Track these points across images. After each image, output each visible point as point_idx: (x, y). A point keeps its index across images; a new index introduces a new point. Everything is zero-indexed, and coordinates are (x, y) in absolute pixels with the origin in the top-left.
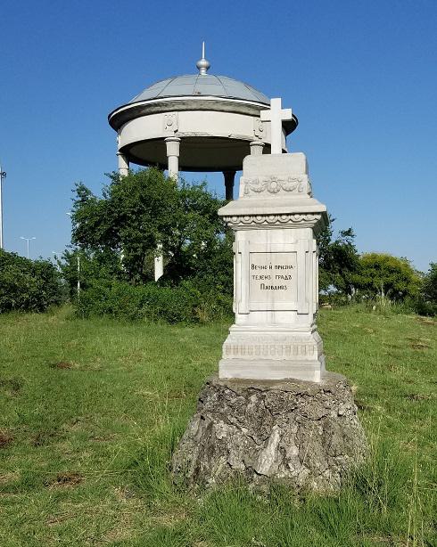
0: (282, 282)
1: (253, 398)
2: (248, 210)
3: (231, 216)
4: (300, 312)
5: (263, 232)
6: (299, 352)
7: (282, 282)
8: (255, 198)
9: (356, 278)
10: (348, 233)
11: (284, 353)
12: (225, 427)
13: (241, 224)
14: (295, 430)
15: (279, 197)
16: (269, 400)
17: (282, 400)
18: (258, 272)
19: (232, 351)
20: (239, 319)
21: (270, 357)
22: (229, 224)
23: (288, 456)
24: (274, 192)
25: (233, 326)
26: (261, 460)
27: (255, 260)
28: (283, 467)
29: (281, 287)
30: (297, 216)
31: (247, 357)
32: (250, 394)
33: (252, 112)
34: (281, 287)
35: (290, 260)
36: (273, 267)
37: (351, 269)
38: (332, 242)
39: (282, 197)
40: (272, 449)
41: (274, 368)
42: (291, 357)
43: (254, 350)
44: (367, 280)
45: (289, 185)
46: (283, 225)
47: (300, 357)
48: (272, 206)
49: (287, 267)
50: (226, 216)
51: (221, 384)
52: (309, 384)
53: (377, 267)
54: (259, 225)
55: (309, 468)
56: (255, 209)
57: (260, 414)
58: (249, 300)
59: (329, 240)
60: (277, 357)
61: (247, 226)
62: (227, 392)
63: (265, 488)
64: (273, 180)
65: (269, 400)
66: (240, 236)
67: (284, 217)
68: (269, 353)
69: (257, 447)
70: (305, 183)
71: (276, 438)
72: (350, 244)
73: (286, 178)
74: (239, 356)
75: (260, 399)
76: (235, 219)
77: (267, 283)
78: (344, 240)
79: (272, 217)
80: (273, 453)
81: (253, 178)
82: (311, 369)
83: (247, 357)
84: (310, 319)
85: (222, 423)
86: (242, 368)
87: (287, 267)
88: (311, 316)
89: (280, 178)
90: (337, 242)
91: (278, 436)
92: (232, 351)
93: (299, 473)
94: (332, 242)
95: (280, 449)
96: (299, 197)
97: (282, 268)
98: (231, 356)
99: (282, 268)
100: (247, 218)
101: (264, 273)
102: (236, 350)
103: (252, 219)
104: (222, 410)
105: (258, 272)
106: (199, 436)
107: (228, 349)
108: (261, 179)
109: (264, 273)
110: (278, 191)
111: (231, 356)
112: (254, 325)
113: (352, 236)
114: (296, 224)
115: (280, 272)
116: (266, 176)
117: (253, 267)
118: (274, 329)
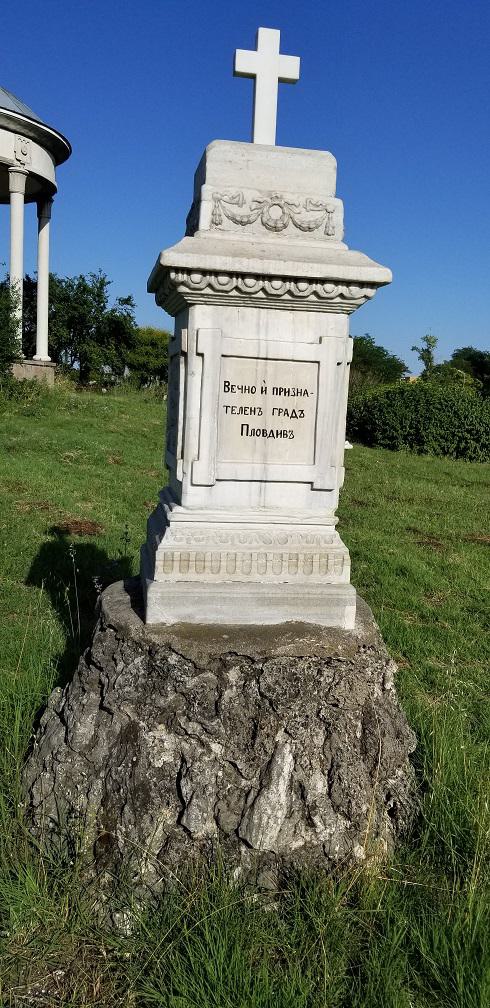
0: (286, 423)
1: (233, 675)
2: (229, 259)
3: (189, 271)
4: (315, 487)
5: (251, 313)
6: (316, 569)
7: (286, 423)
8: (235, 235)
9: (129, 355)
10: (127, 301)
11: (286, 570)
12: (170, 741)
13: (208, 291)
14: (319, 740)
15: (284, 241)
16: (270, 680)
17: (294, 678)
18: (236, 399)
19: (176, 564)
20: (191, 495)
21: (256, 577)
22: (183, 289)
23: (310, 798)
24: (276, 229)
25: (177, 509)
26: (260, 819)
27: (235, 373)
28: (302, 826)
29: (283, 434)
30: (329, 287)
31: (207, 577)
32: (226, 666)
33: (12, 126)
34: (283, 434)
35: (304, 377)
36: (270, 391)
37: (131, 347)
38: (109, 308)
39: (291, 239)
40: (279, 792)
41: (265, 602)
42: (300, 577)
43: (223, 564)
44: (142, 359)
45: (306, 217)
46: (296, 302)
47: (316, 578)
48: (279, 257)
49: (298, 393)
50: (178, 270)
51: (156, 639)
52: (335, 633)
53: (154, 344)
54: (247, 299)
55: (348, 817)
56: (245, 261)
57: (251, 713)
58: (215, 459)
59: (104, 307)
60: (271, 578)
61: (220, 298)
62: (173, 659)
63: (269, 879)
64: (276, 201)
65: (270, 680)
66: (201, 317)
67: (303, 285)
68: (254, 570)
69: (244, 782)
70: (338, 218)
71: (286, 763)
72: (129, 315)
73: (302, 200)
74: (192, 576)
75: (247, 678)
76: (196, 277)
77: (255, 422)
78: (122, 310)
79: (277, 284)
80: (283, 799)
81: (233, 192)
82: (339, 602)
83: (207, 577)
84: (332, 501)
85: (161, 731)
86: (200, 601)
87: (298, 393)
88: (336, 493)
89: (289, 198)
90: (113, 311)
91: (289, 758)
92: (176, 564)
93: (330, 829)
94: (109, 308)
95: (299, 789)
96: (323, 245)
97: (287, 392)
98: (176, 576)
99: (287, 392)
100: (224, 279)
101: (248, 400)
102: (185, 562)
103: (236, 282)
104: (162, 702)
105: (236, 399)
106: (102, 752)
107: (169, 560)
108: (250, 195)
109: (248, 400)
110: (285, 226)
111: (176, 576)
112: (225, 508)
113: (132, 306)
114: (323, 304)
115: (281, 401)
116: (260, 191)
117: (228, 387)
118: (263, 519)
